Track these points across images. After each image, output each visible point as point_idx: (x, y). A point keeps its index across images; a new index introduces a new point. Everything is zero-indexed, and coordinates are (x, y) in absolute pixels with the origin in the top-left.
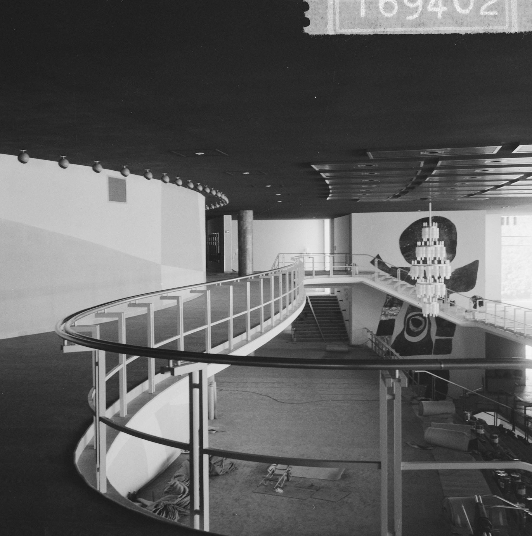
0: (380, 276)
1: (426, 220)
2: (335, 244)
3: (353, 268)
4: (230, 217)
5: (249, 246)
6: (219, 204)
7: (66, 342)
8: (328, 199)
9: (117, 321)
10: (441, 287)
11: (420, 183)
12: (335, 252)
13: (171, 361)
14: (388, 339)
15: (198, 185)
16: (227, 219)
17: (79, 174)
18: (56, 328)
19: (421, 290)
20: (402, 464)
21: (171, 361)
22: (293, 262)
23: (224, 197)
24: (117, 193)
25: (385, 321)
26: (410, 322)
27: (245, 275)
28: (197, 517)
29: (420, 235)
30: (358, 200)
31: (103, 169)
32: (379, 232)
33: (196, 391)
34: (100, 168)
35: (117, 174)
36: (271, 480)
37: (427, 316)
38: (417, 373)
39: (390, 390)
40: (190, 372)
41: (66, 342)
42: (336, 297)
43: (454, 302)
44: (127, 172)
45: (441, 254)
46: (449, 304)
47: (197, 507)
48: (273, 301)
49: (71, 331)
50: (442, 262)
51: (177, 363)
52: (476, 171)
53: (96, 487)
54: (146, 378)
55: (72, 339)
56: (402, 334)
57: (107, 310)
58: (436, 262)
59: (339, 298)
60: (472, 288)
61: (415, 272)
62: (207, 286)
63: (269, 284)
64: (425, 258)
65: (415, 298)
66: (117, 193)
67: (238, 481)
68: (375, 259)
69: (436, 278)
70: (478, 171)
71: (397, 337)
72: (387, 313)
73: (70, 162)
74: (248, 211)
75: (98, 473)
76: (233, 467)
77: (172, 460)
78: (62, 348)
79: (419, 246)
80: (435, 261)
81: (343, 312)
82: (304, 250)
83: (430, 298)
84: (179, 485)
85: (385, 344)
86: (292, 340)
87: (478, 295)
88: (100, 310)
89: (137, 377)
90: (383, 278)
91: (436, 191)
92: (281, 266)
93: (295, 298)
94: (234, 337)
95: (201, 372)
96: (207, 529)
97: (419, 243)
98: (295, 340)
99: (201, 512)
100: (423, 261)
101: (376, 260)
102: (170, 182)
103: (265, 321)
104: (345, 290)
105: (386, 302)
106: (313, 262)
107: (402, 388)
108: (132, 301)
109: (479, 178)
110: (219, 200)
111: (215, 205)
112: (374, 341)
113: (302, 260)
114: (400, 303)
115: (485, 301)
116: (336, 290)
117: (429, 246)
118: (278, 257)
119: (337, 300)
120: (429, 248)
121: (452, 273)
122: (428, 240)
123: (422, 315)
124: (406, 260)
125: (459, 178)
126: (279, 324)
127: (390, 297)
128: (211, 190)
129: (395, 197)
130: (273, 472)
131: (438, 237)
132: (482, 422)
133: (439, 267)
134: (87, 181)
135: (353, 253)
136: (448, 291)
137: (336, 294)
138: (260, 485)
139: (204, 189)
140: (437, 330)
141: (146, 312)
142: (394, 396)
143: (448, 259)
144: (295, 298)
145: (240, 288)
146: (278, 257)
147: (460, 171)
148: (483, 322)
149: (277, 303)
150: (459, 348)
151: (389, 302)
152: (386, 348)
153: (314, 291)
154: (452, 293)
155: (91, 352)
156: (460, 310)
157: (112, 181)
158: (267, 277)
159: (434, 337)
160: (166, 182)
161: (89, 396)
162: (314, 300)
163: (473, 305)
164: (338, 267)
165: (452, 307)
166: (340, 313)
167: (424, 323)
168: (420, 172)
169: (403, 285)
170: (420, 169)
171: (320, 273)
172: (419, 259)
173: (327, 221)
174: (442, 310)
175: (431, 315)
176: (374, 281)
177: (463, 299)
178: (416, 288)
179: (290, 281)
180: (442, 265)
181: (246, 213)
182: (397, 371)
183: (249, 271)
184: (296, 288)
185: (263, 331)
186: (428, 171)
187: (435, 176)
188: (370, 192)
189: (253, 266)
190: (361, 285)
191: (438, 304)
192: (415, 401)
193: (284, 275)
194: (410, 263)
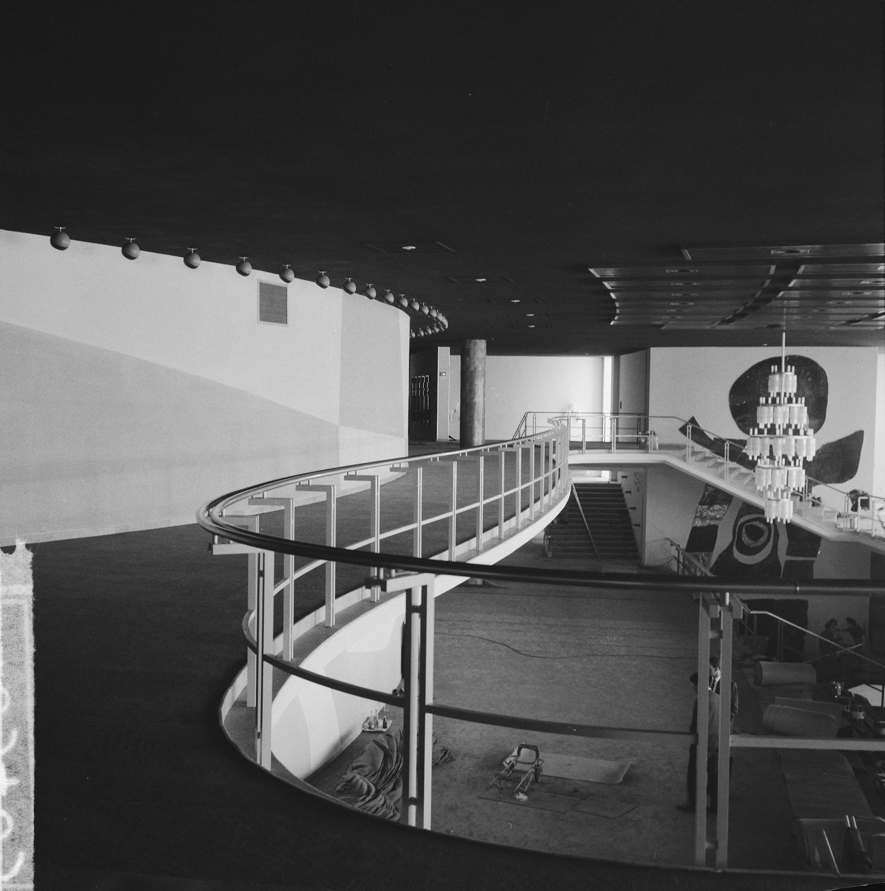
0: (694, 453)
1: (777, 361)
2: (622, 398)
3: (650, 438)
4: (447, 349)
5: (479, 399)
6: (432, 329)
7: (216, 537)
8: (612, 323)
9: (282, 512)
10: (799, 473)
11: (768, 300)
12: (621, 411)
13: (382, 570)
14: (706, 558)
15: (400, 298)
16: (444, 353)
17: (217, 276)
18: (198, 518)
19: (764, 478)
20: (731, 738)
21: (382, 570)
22: (551, 426)
23: (442, 318)
24: (273, 308)
25: (701, 528)
26: (744, 530)
27: (470, 445)
28: (413, 809)
29: (766, 386)
30: (663, 325)
31: (73, 241)
32: (696, 379)
33: (416, 618)
34: (248, 268)
35: (273, 279)
36: (507, 780)
37: (772, 522)
38: (753, 615)
39: (715, 624)
40: (408, 587)
41: (216, 537)
42: (620, 485)
43: (819, 499)
44: (291, 275)
45: (800, 419)
46: (811, 503)
47: (413, 793)
48: (531, 483)
49: (221, 521)
50: (802, 432)
51: (390, 573)
52: (863, 282)
53: (256, 760)
54: (322, 603)
55: (224, 534)
56: (729, 550)
57: (268, 494)
58: (791, 431)
59: (625, 488)
60: (851, 477)
61: (755, 448)
62: (409, 462)
63: (498, 465)
64: (773, 426)
65: (754, 491)
66: (273, 308)
67: (455, 780)
68: (687, 424)
69: (790, 459)
70: (867, 282)
71: (720, 556)
72: (705, 514)
73: (141, 249)
74: (478, 341)
75: (259, 740)
76: (447, 756)
77: (348, 742)
78: (210, 548)
79: (763, 405)
80: (790, 429)
81: (631, 511)
82: (569, 407)
83: (778, 492)
84: (361, 781)
85: (700, 565)
86: (544, 555)
87: (860, 488)
88: (257, 494)
89: (310, 598)
90: (700, 456)
91: (793, 314)
92: (529, 432)
93: (554, 485)
94: (457, 544)
95: (424, 589)
96: (427, 825)
97: (762, 400)
98: (550, 555)
99: (419, 801)
100: (768, 430)
101: (690, 426)
102: (357, 292)
103: (505, 520)
104: (636, 474)
105: (703, 497)
106: (584, 427)
107: (734, 620)
108: (303, 481)
109: (867, 293)
110: (435, 322)
111: (425, 331)
112: (681, 560)
113: (565, 423)
114: (726, 498)
115: (871, 500)
116: (620, 474)
117: (780, 404)
118: (525, 417)
119: (621, 490)
120: (779, 409)
121: (817, 452)
122: (779, 394)
123: (763, 520)
124: (740, 428)
125: (834, 293)
126: (528, 526)
127: (710, 489)
128: (421, 306)
129: (724, 322)
130: (512, 766)
131: (795, 391)
132: (861, 701)
133: (796, 441)
134: (226, 289)
135: (651, 412)
136: (810, 482)
137: (620, 481)
138: (491, 787)
139: (410, 304)
140: (789, 546)
141: (325, 499)
142: (720, 633)
143: (810, 427)
144: (554, 485)
145: (468, 466)
146: (525, 417)
147: (836, 282)
148: (867, 535)
149: (525, 492)
150: (823, 566)
151: (709, 495)
152: (702, 572)
153: (584, 475)
154: (816, 484)
155: (246, 556)
156: (828, 513)
157: (265, 288)
158: (510, 450)
159: (783, 557)
160: (350, 293)
161: (244, 623)
162: (581, 488)
163: (851, 505)
164: (623, 437)
165: (815, 508)
166: (627, 512)
167: (766, 533)
168: (768, 282)
169: (732, 470)
170: (769, 277)
171: (592, 446)
172: (762, 426)
173: (608, 360)
174: (797, 512)
175: (779, 520)
176: (685, 461)
177: (833, 496)
178: (756, 475)
179: (547, 458)
180: (801, 437)
181: (475, 344)
182: (728, 594)
183: (478, 439)
184: (556, 469)
185: (503, 537)
186: (782, 282)
187: (793, 289)
188: (685, 314)
189: (484, 432)
190: (663, 468)
191: (792, 502)
192: (748, 662)
193: (537, 447)
194: (748, 433)
